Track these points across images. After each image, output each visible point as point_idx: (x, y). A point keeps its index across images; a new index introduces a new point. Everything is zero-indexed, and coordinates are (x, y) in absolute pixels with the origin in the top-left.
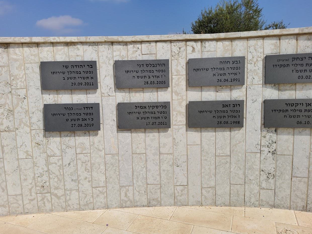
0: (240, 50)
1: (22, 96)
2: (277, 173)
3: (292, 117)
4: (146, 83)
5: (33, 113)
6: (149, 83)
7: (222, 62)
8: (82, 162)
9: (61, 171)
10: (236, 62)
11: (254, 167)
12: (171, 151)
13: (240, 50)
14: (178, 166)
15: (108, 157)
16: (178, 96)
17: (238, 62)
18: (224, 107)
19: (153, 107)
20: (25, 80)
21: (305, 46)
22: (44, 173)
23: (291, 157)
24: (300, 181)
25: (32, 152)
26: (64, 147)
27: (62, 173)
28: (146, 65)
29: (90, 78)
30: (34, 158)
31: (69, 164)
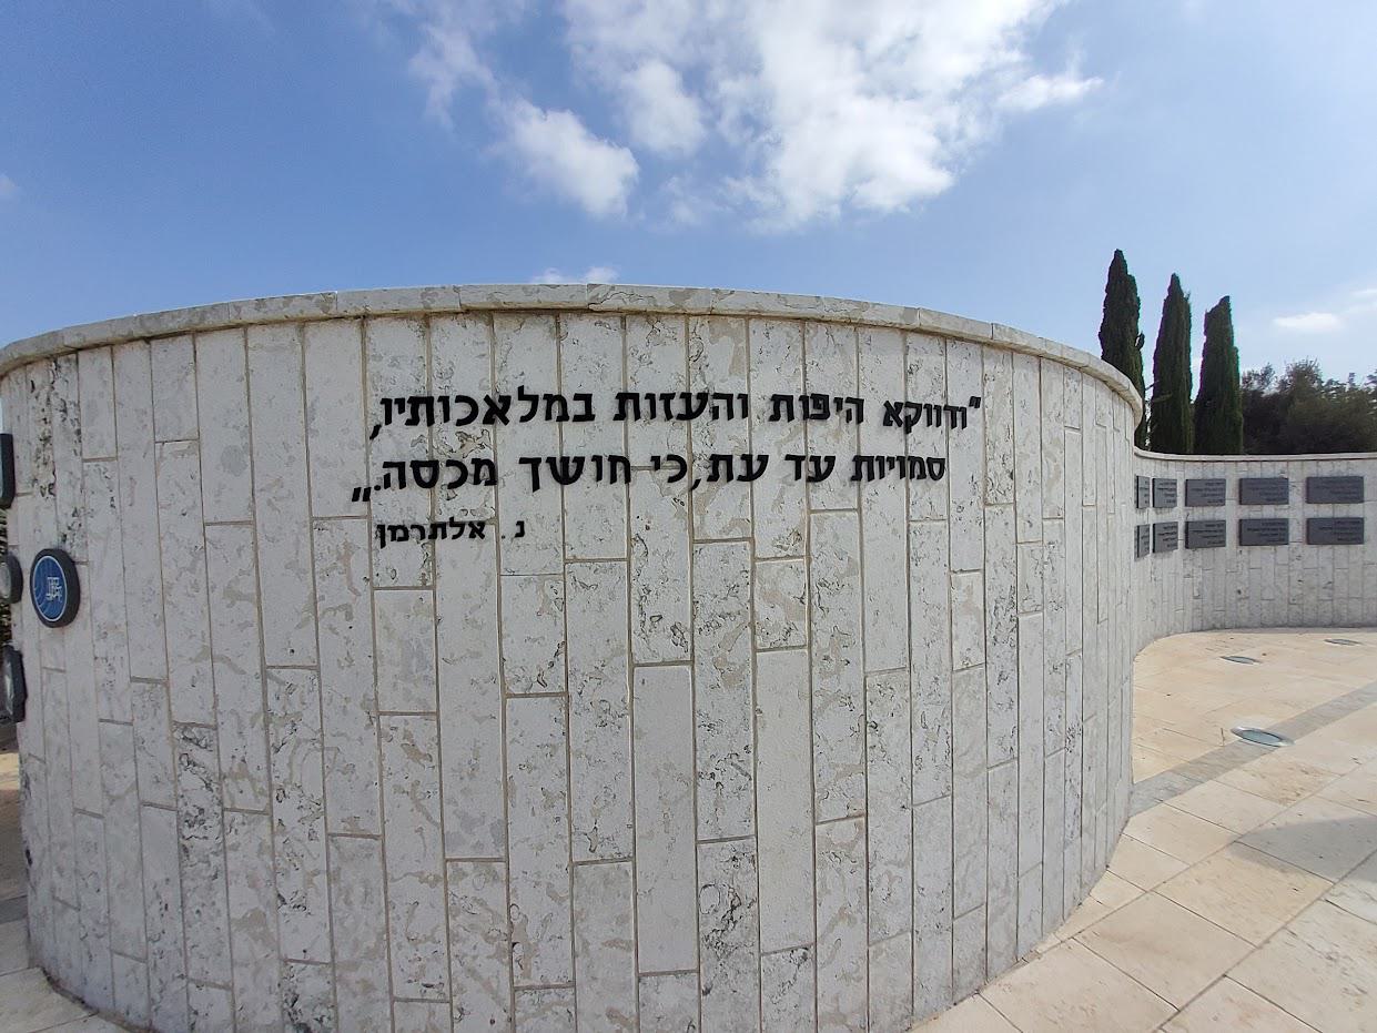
16: (1296, 511)
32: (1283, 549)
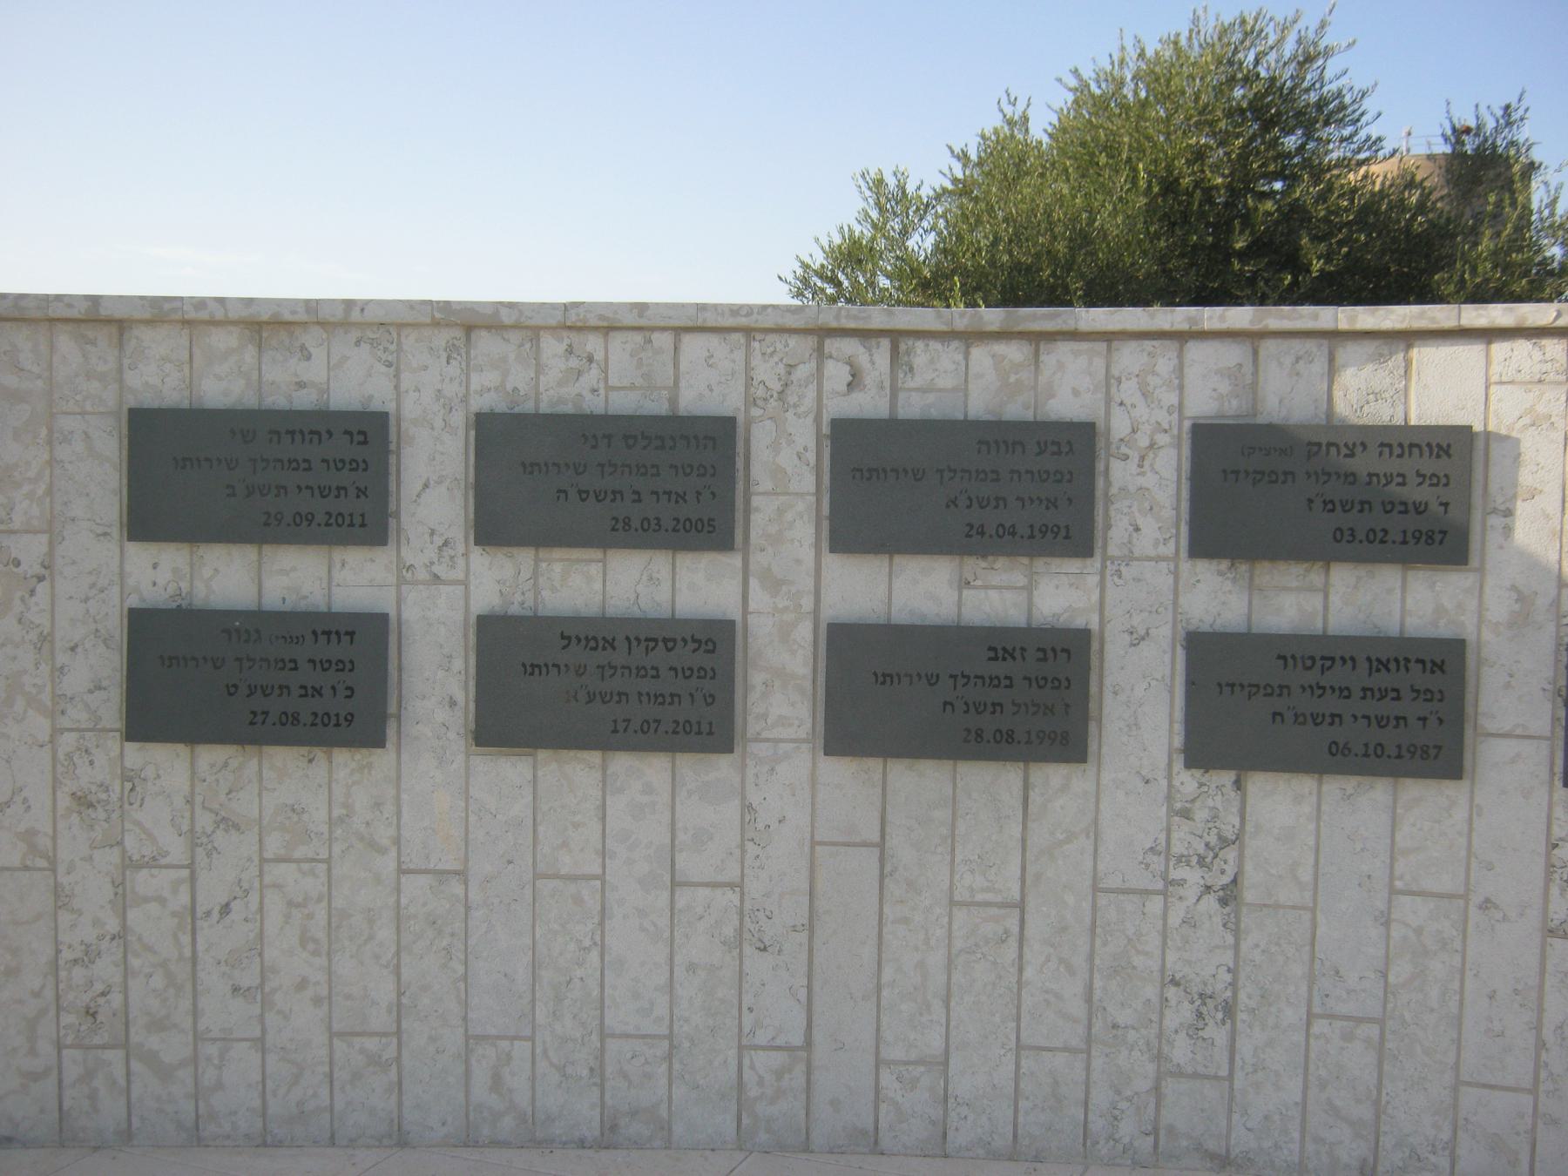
0: (1076, 393)
1: (31, 566)
2: (1242, 996)
3: (1309, 719)
4: (620, 525)
5: (73, 649)
6: (635, 523)
7: (987, 443)
8: (290, 904)
9: (186, 939)
10: (1055, 448)
11: (1138, 961)
12: (733, 873)
13: (1076, 393)
14: (765, 949)
15: (415, 886)
17: (1065, 449)
18: (996, 659)
19: (652, 644)
20: (50, 491)
21: (1363, 387)
22: (105, 944)
23: (1307, 916)
24: (1348, 1037)
25: (54, 838)
26: (205, 821)
27: (187, 952)
28: (626, 437)
29: (352, 492)
30: (61, 870)
31: (226, 909)
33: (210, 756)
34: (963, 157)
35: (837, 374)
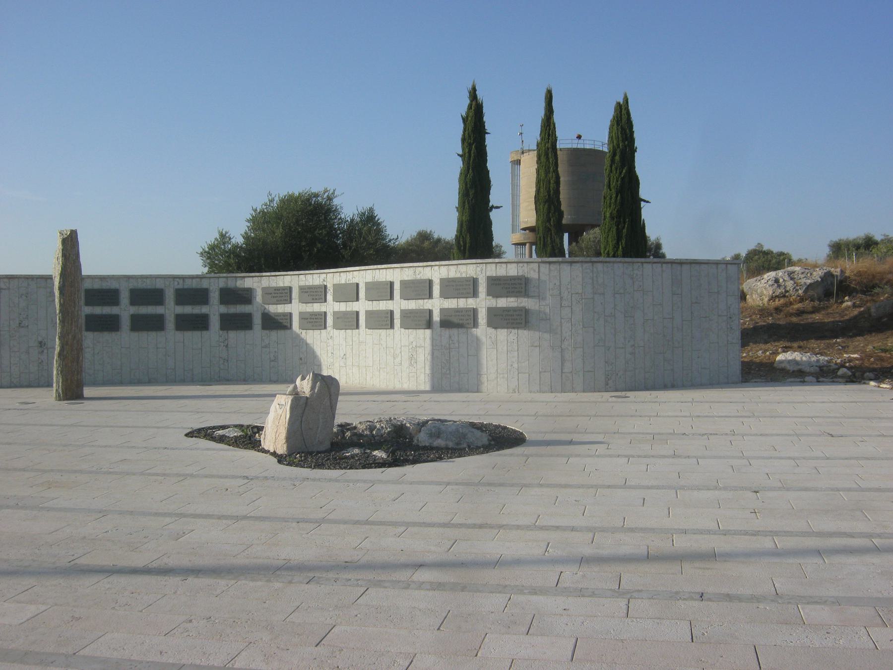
32: (323, 331)
33: (96, 333)
34: (255, 210)
35: (176, 283)
